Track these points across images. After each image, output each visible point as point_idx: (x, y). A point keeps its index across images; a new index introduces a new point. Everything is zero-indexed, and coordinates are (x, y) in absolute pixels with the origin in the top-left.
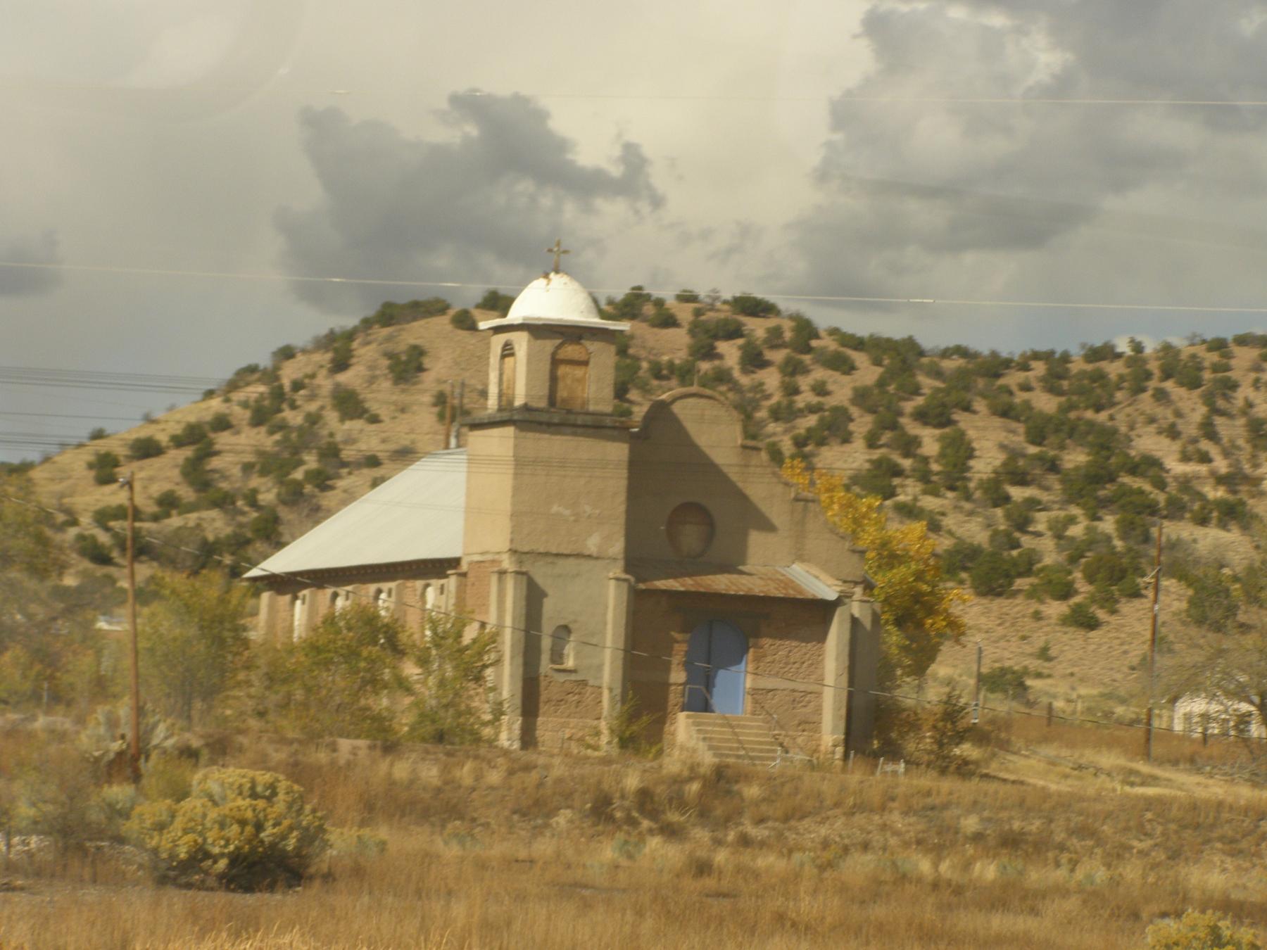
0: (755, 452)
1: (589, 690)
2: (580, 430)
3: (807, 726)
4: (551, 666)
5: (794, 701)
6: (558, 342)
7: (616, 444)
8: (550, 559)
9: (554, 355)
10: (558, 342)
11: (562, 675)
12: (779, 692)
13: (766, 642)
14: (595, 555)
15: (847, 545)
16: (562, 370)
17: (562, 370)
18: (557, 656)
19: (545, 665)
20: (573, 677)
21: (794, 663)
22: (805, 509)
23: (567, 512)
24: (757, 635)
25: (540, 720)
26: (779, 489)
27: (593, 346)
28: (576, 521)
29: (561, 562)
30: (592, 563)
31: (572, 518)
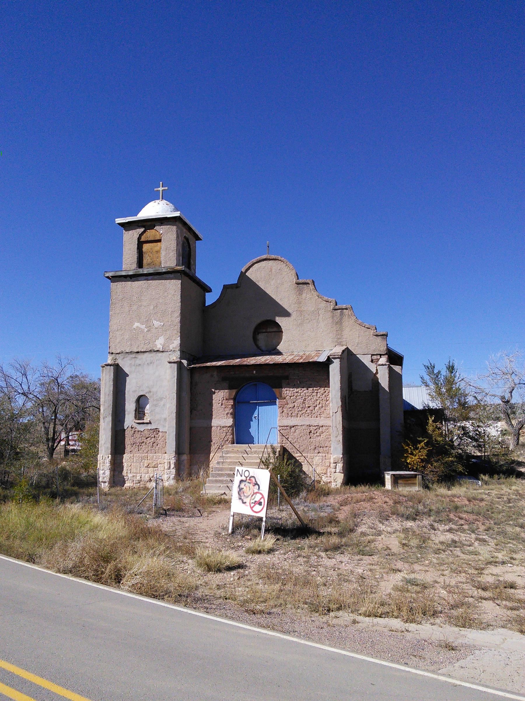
0: (305, 286)
1: (160, 434)
2: (150, 277)
3: (321, 450)
4: (134, 421)
5: (311, 432)
6: (142, 230)
7: (173, 281)
8: (133, 355)
9: (139, 239)
10: (142, 230)
11: (142, 425)
12: (299, 427)
13: (287, 392)
14: (161, 350)
15: (372, 332)
16: (146, 247)
17: (146, 247)
18: (140, 413)
19: (129, 420)
20: (149, 427)
21: (309, 407)
22: (342, 314)
23: (143, 327)
24: (432, 409)
25: (126, 457)
26: (324, 304)
27: (161, 230)
28: (149, 331)
29: (140, 356)
30: (160, 354)
31: (146, 330)
